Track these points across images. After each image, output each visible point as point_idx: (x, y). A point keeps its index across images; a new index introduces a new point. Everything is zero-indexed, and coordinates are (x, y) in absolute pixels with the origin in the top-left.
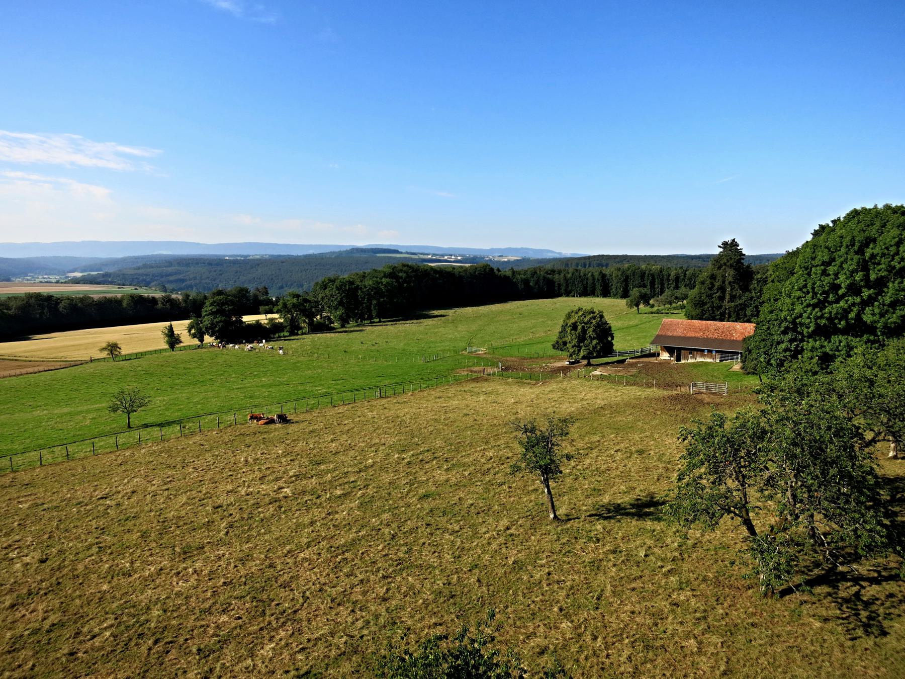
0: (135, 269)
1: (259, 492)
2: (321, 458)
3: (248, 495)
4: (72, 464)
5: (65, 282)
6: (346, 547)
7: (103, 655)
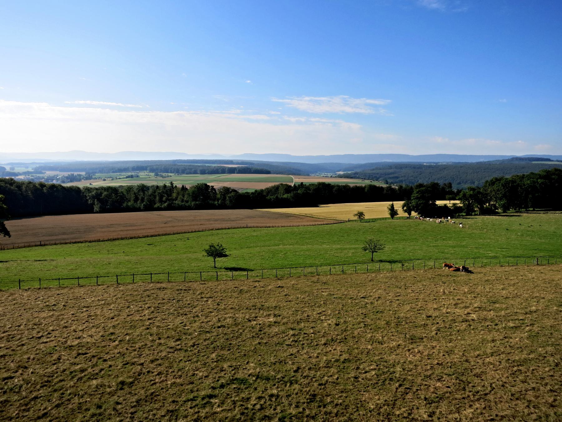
0: (371, 170)
1: (454, 313)
2: (495, 299)
3: (447, 313)
4: (345, 276)
5: (335, 177)
6: (521, 363)
7: (372, 384)
